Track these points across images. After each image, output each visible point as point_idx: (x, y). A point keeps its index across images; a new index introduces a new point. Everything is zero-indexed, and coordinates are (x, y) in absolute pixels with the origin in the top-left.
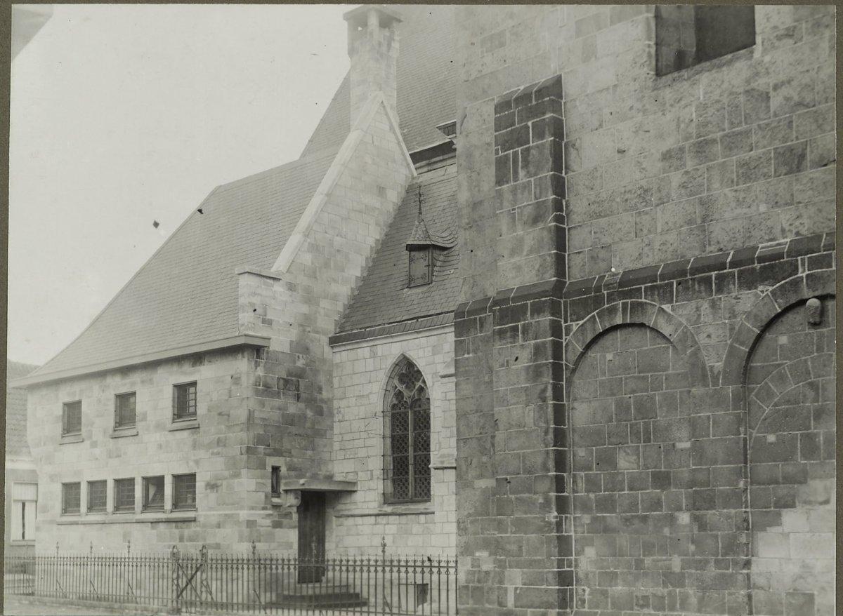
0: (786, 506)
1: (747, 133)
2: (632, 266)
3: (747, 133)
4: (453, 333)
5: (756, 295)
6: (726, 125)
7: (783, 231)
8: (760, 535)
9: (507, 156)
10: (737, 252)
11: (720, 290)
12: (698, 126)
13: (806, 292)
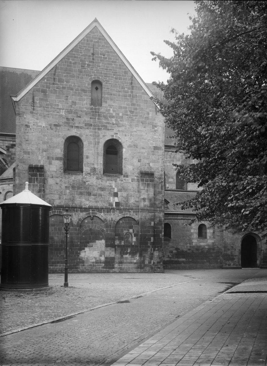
0: (86, 247)
1: (82, 187)
2: (58, 204)
3: (82, 187)
4: (49, 279)
5: (83, 214)
6: (78, 185)
7: (87, 204)
8: (81, 251)
9: (32, 178)
10: (79, 206)
11: (76, 212)
12: (73, 183)
13: (91, 215)
